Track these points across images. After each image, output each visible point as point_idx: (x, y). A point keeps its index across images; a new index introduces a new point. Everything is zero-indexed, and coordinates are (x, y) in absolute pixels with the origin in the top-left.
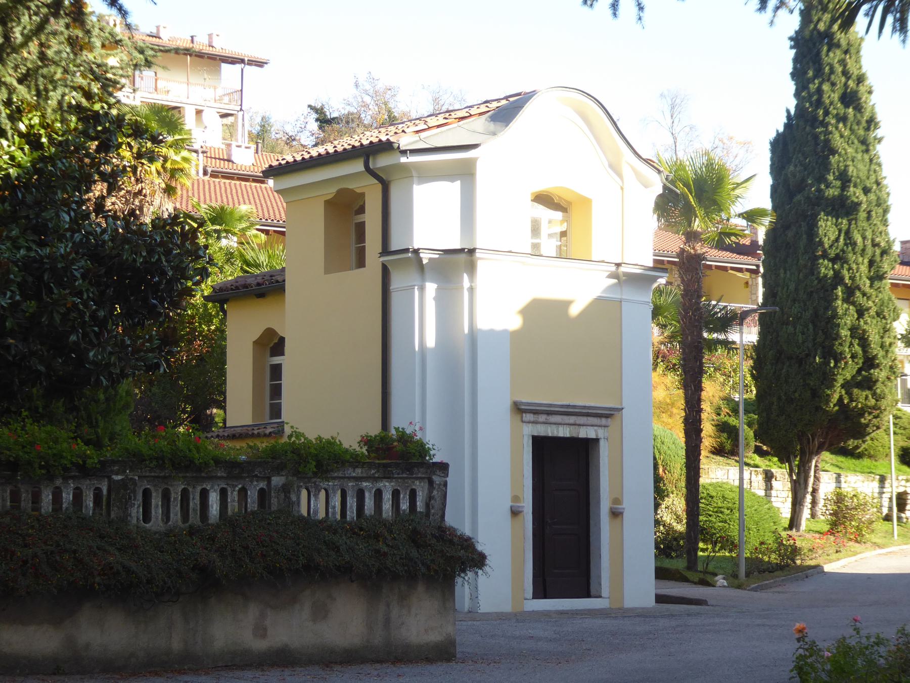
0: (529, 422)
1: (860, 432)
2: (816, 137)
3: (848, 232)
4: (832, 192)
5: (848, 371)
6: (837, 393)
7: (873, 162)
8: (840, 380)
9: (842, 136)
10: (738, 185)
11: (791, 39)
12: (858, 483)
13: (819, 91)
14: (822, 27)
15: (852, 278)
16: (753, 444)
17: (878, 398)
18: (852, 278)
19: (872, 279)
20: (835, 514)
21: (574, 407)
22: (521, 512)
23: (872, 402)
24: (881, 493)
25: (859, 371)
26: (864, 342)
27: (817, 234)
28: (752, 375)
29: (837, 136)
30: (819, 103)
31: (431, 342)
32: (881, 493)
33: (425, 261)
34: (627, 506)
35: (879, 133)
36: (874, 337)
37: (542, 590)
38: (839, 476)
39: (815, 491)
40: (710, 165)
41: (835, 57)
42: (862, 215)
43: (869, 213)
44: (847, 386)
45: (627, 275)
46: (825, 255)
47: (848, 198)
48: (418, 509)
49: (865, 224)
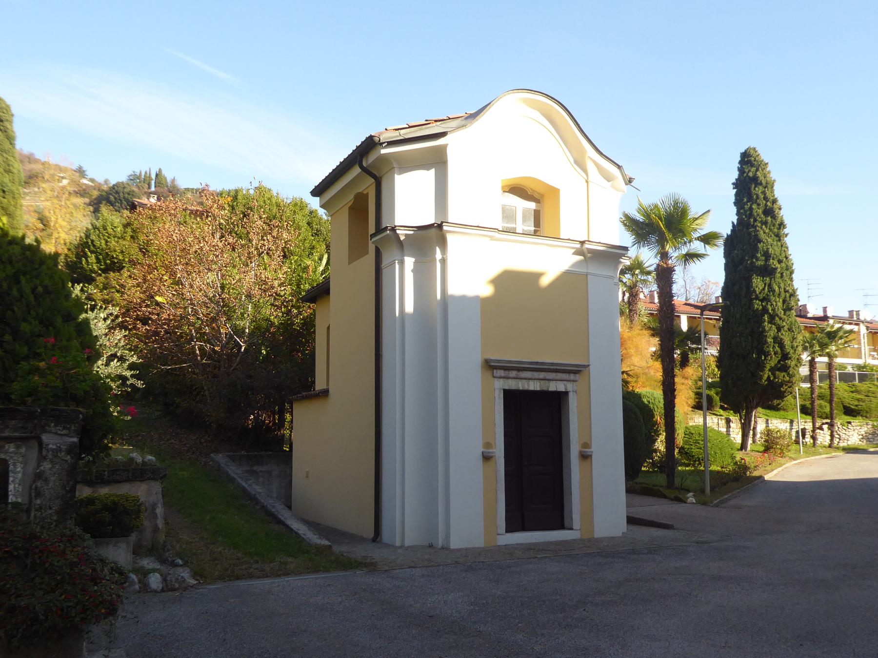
0: (500, 378)
1: (781, 396)
2: (749, 234)
3: (770, 285)
4: (760, 263)
5: (773, 361)
6: (766, 374)
7: (784, 247)
8: (768, 367)
9: (764, 233)
10: (696, 219)
11: (733, 184)
12: (779, 425)
13: (751, 209)
14: (751, 174)
15: (773, 310)
16: (719, 404)
17: (791, 376)
18: (773, 310)
19: (785, 310)
20: (766, 441)
21: (543, 364)
22: (492, 457)
23: (788, 378)
24: (791, 429)
25: (779, 362)
26: (782, 345)
27: (752, 286)
28: (717, 366)
29: (762, 232)
30: (751, 215)
31: (409, 308)
32: (791, 429)
33: (402, 238)
34: (595, 450)
35: (786, 231)
36: (787, 342)
37: (512, 526)
38: (767, 421)
39: (754, 428)
40: (676, 203)
41: (759, 190)
42: (778, 275)
43: (782, 274)
44: (772, 370)
45: (591, 251)
46: (757, 298)
47: (769, 265)
48: (11, 499)
49: (780, 280)
